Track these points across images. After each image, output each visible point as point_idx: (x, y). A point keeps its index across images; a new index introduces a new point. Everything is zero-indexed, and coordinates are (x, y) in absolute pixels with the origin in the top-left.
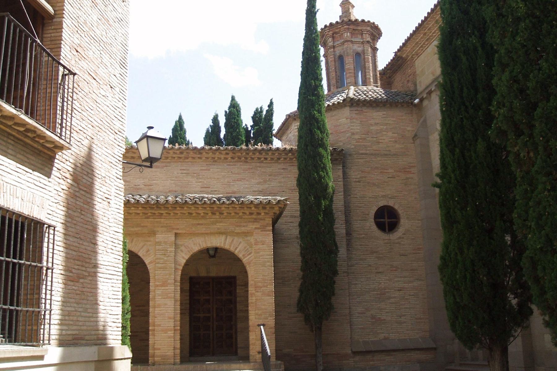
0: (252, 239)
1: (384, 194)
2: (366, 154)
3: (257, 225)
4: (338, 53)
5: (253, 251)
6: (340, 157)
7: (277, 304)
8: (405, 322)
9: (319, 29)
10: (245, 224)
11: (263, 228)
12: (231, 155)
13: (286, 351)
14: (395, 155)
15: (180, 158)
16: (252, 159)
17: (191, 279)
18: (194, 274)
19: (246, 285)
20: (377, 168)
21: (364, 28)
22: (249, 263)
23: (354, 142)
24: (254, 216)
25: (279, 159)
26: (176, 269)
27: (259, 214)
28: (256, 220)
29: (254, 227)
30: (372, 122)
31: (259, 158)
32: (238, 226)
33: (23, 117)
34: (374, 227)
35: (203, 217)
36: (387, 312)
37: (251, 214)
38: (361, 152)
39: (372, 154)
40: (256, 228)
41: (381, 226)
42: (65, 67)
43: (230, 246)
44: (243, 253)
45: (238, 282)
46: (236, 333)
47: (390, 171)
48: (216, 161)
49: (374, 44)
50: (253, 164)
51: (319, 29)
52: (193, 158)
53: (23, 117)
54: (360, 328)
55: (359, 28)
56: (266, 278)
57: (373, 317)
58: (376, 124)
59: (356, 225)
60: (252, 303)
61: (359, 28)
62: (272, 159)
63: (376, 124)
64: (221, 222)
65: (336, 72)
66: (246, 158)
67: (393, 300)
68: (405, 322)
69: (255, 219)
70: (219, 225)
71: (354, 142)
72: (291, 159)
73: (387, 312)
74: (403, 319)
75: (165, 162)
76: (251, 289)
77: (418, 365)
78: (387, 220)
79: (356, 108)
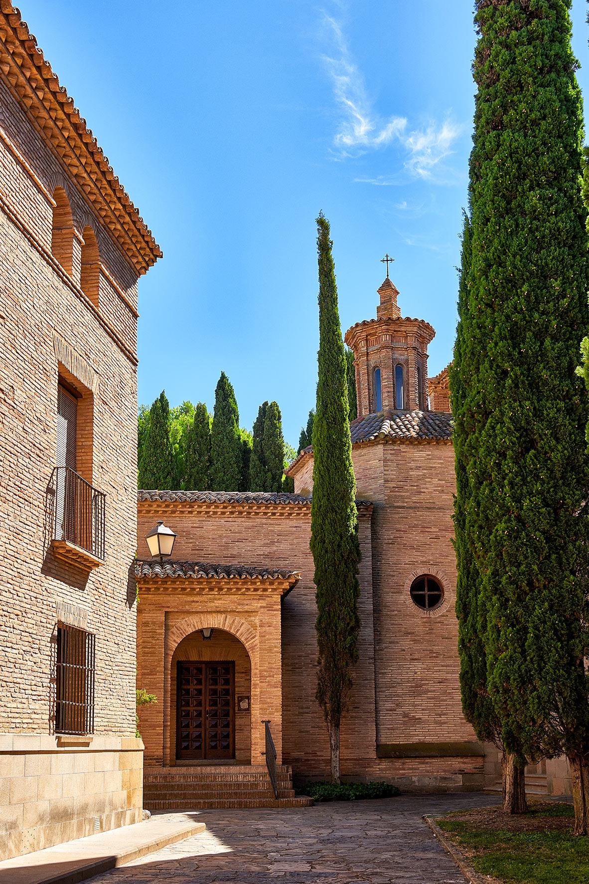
0: (257, 620)
1: (424, 559)
2: (403, 507)
3: (262, 603)
4: (372, 363)
5: (258, 634)
6: (372, 511)
7: (285, 697)
8: (445, 723)
9: (223, 849)
10: (248, 602)
11: (269, 607)
12: (229, 509)
13: (295, 754)
14: (440, 508)
15: (166, 512)
16: (257, 514)
17: (179, 663)
18: (183, 659)
19: (248, 672)
20: (416, 526)
21: (409, 329)
22: (253, 648)
23: (388, 492)
24: (259, 593)
25: (290, 514)
26: (166, 654)
27: (265, 590)
28: (261, 597)
29: (259, 605)
30: (413, 465)
31: (265, 514)
32: (239, 604)
33: (78, 549)
34: (410, 601)
35: (199, 594)
36: (423, 710)
37: (256, 590)
38: (396, 504)
39: (410, 508)
40: (261, 607)
41: (419, 600)
42: (95, 490)
43: (231, 628)
44: (245, 636)
45: (236, 668)
46: (234, 730)
47: (433, 530)
48: (210, 516)
49: (423, 351)
50: (258, 520)
51: (223, 849)
52: (182, 512)
53: (78, 549)
54: (388, 729)
55: (403, 329)
56: (273, 666)
57: (405, 715)
58: (418, 468)
59: (389, 598)
60: (255, 695)
61: (403, 329)
62: (282, 514)
63: (418, 468)
64: (219, 599)
65: (369, 389)
66: (249, 513)
67: (430, 695)
68: (445, 723)
69: (261, 596)
70: (217, 603)
71: (388, 492)
72: (306, 514)
73: (423, 710)
74: (443, 718)
75: (146, 517)
76: (255, 680)
77: (461, 776)
78: (426, 592)
79: (392, 447)
